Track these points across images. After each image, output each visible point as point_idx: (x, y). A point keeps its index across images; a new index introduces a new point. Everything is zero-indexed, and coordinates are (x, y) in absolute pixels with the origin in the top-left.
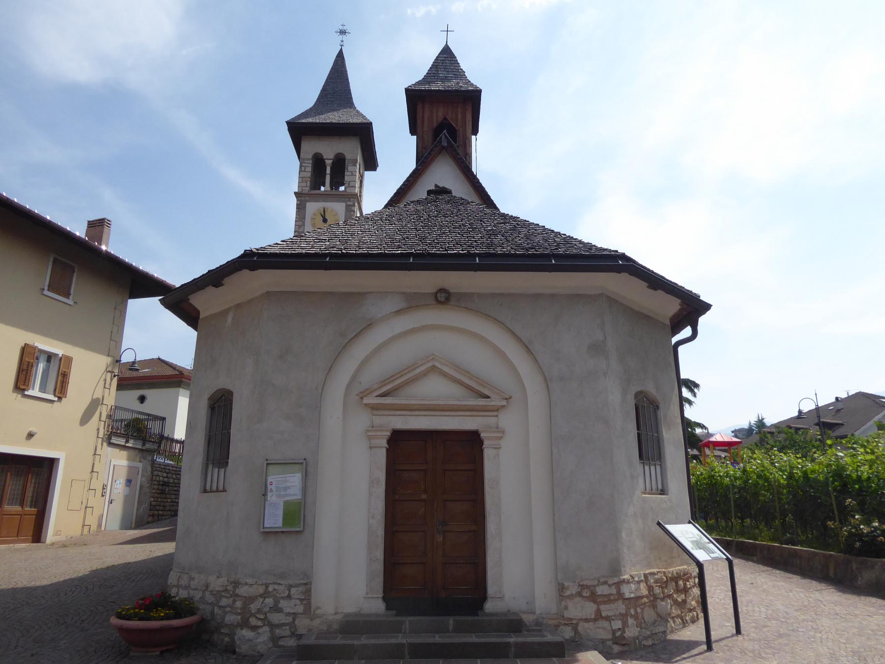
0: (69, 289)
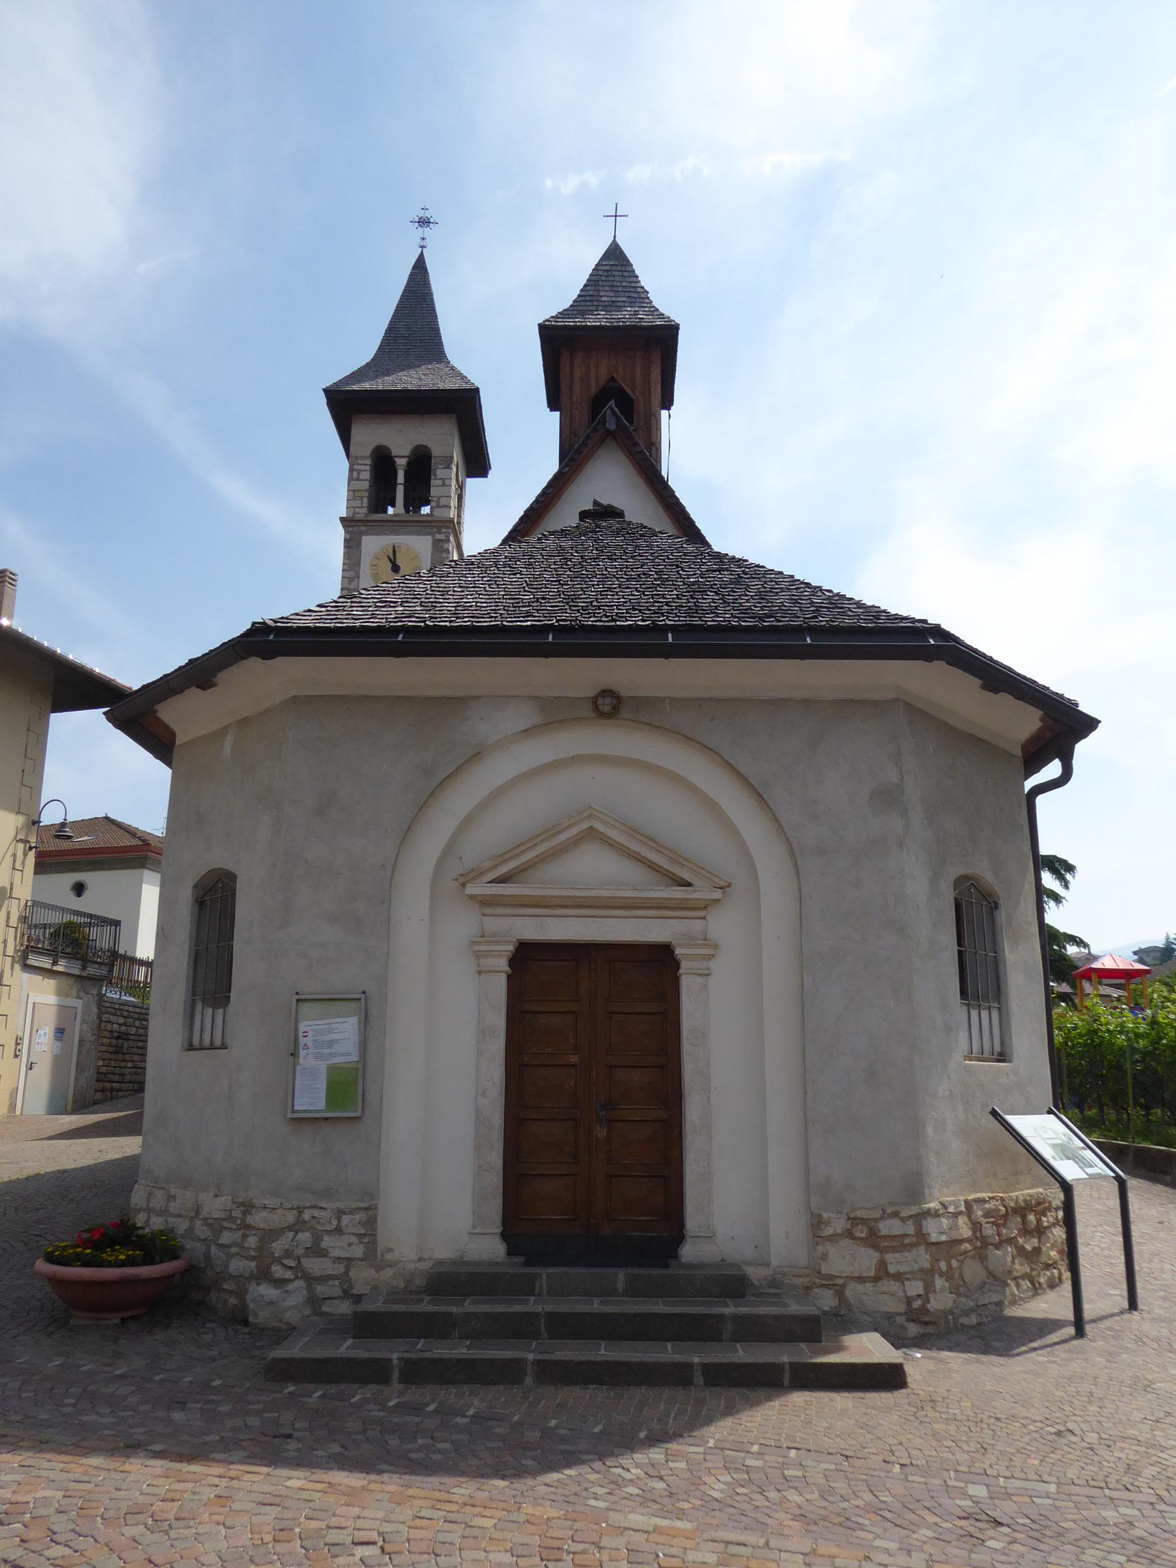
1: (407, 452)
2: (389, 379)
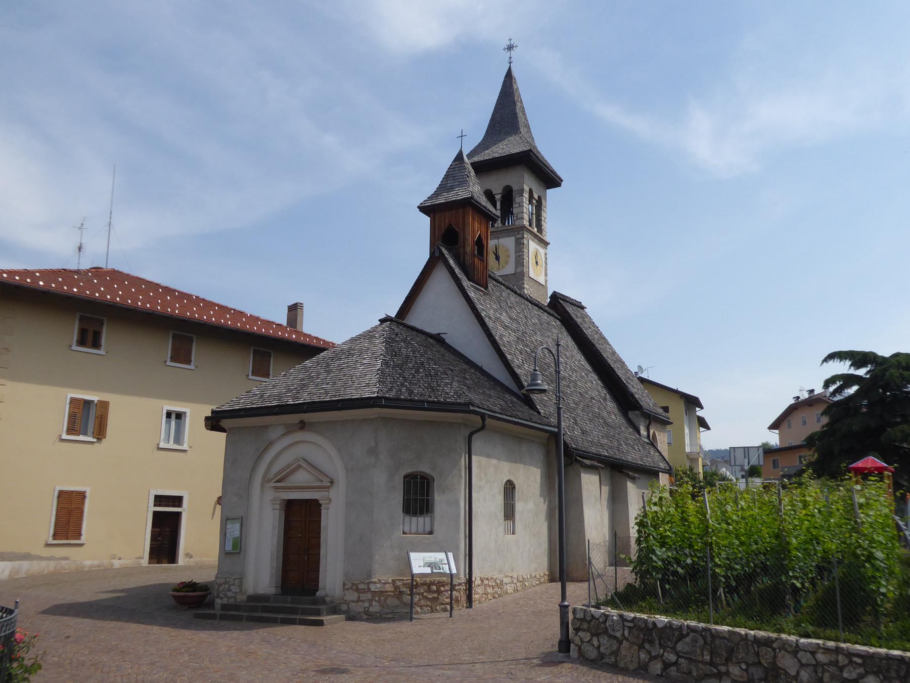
0: (269, 371)
1: (500, 191)
2: (494, 148)
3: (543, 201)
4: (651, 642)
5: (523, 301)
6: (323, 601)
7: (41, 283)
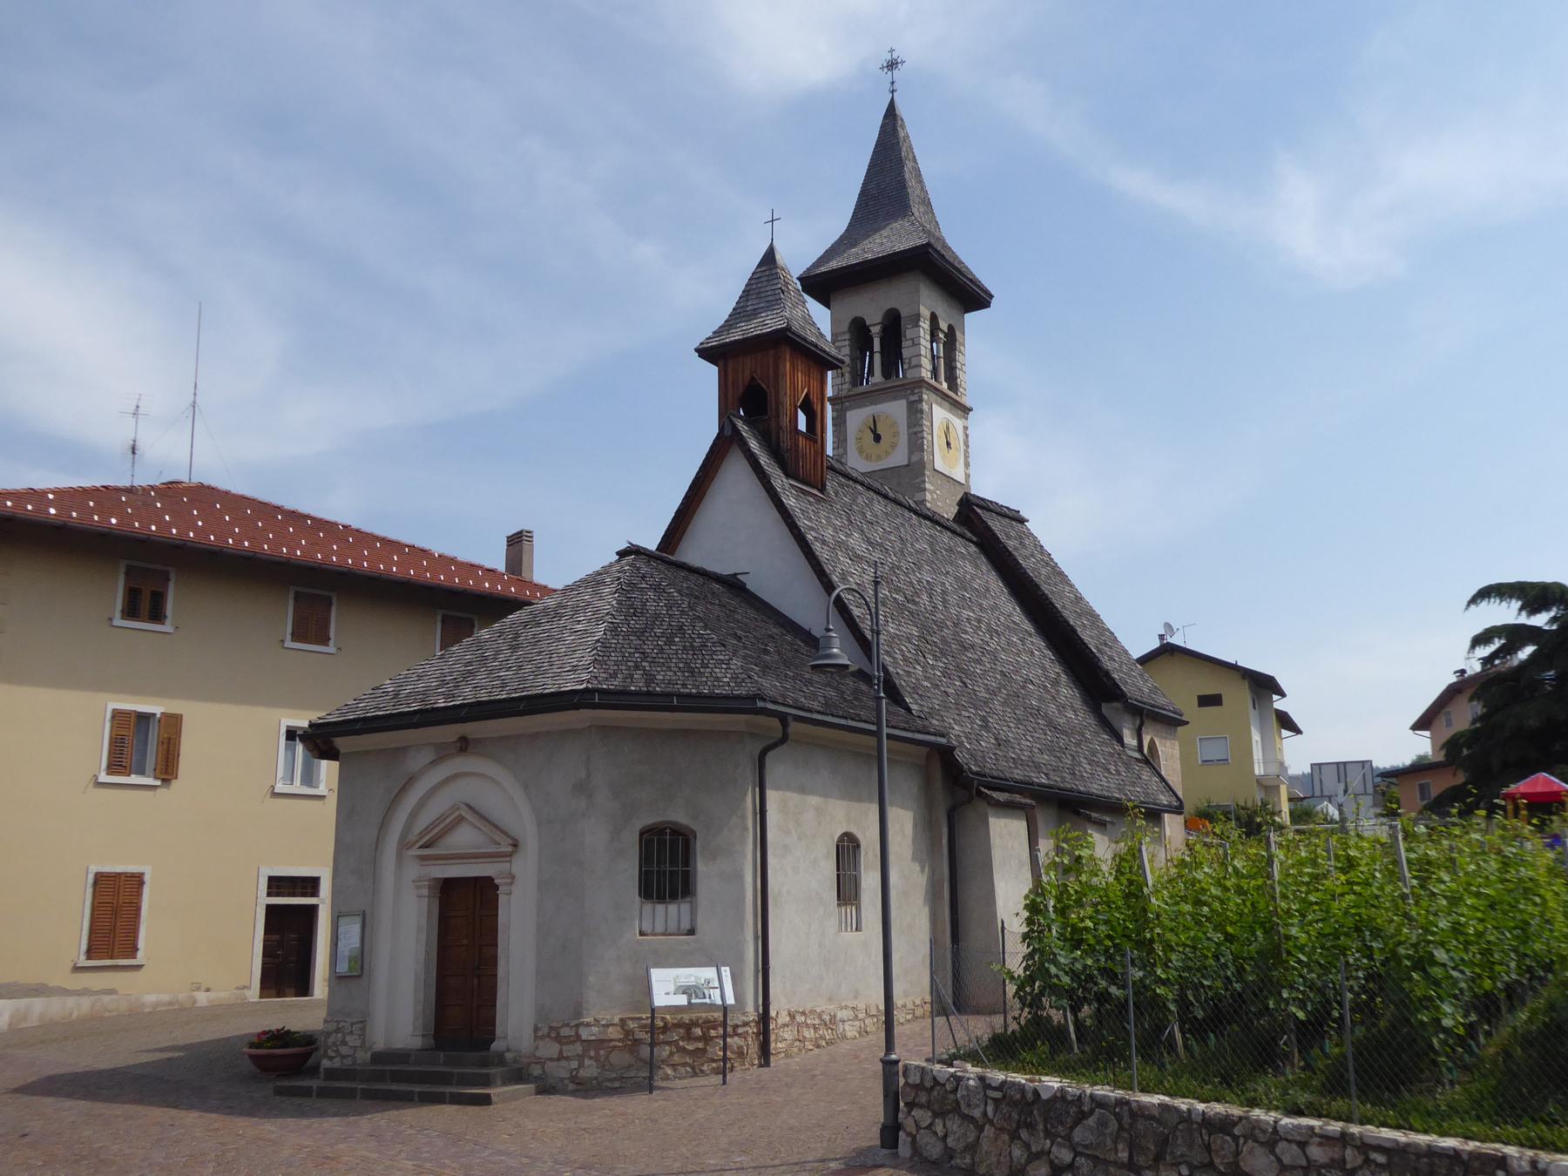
2: (877, 238)
3: (958, 334)
4: (1031, 1127)
5: (899, 510)
6: (500, 1059)
7: (52, 511)
